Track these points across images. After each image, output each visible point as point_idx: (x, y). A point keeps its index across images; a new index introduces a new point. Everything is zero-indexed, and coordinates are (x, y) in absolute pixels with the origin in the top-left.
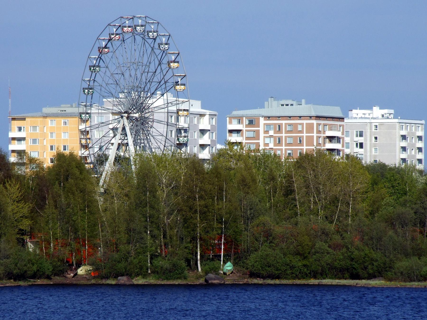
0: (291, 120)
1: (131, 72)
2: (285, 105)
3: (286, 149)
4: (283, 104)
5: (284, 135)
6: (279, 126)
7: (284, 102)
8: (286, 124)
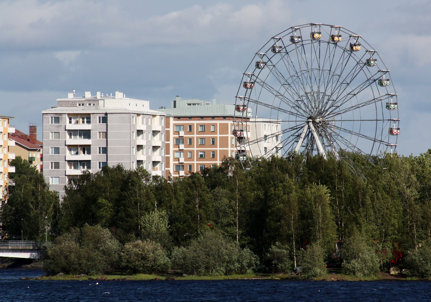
0: (214, 120)
1: (302, 56)
2: (192, 104)
3: (197, 151)
4: (190, 103)
5: (195, 136)
6: (190, 126)
7: (190, 101)
8: (197, 124)
